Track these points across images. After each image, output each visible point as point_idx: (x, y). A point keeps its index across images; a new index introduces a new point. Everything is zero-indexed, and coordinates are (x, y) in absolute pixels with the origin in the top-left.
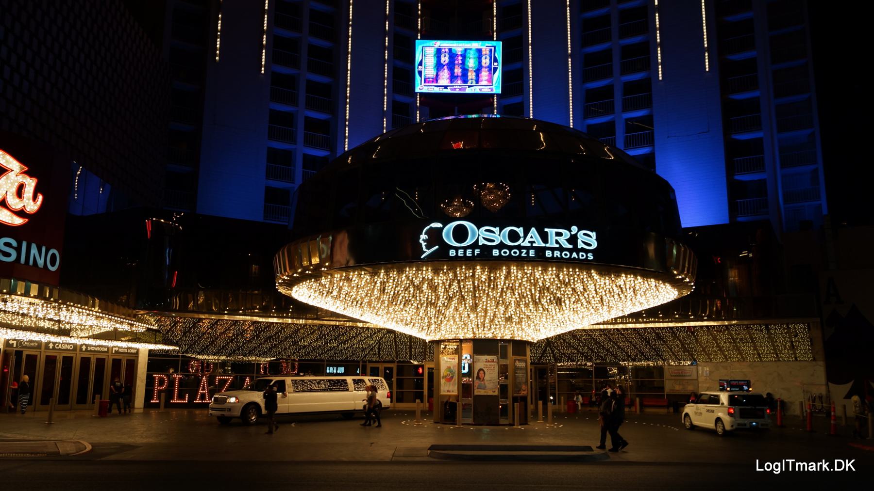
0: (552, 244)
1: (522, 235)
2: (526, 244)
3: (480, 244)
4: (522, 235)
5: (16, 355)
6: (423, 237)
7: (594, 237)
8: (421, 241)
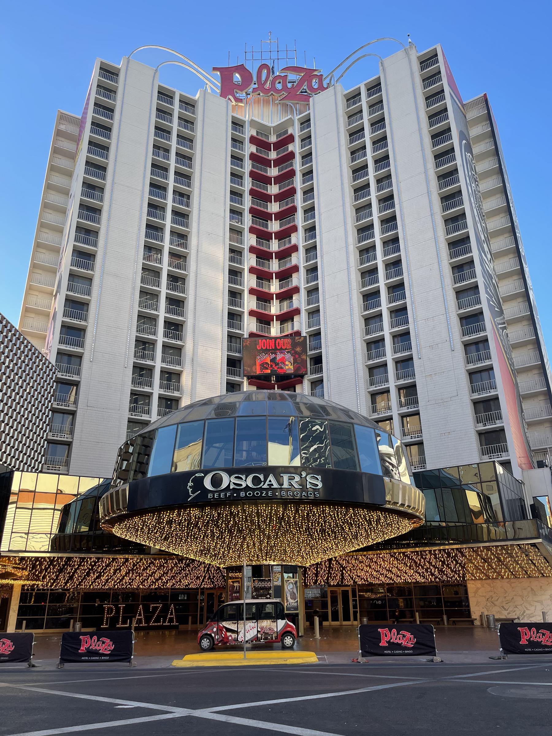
0: (286, 485)
1: (262, 480)
2: (266, 486)
3: (231, 487)
4: (262, 480)
5: (1, 584)
6: (190, 484)
7: (320, 479)
8: (188, 488)
